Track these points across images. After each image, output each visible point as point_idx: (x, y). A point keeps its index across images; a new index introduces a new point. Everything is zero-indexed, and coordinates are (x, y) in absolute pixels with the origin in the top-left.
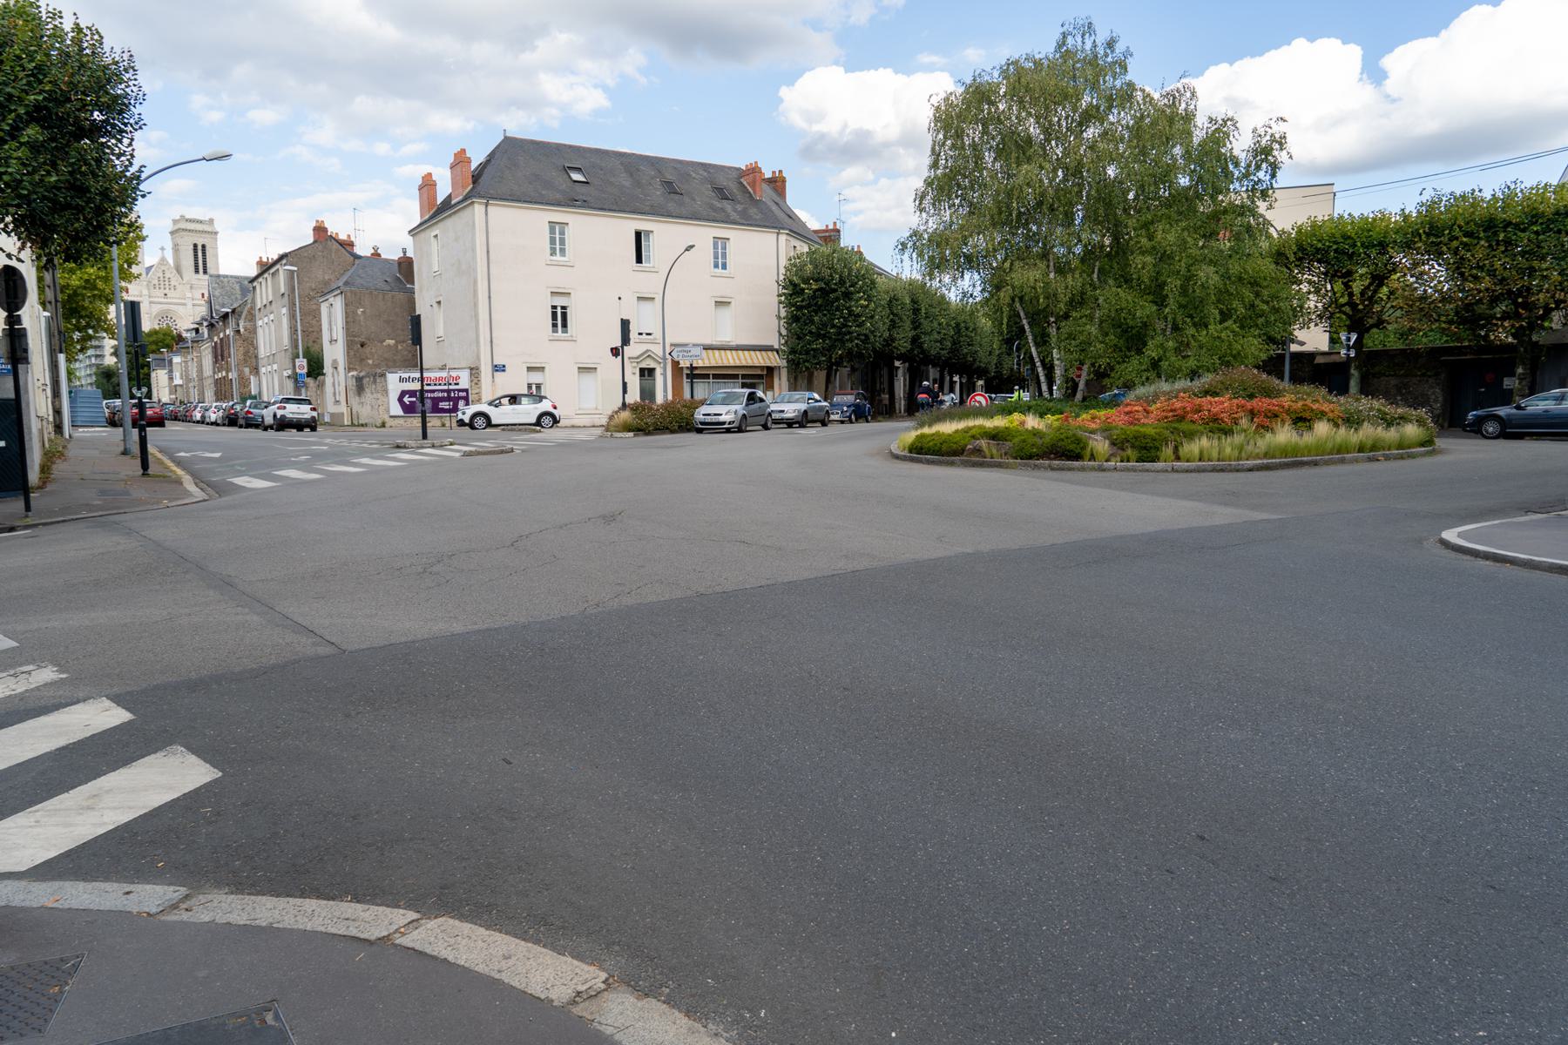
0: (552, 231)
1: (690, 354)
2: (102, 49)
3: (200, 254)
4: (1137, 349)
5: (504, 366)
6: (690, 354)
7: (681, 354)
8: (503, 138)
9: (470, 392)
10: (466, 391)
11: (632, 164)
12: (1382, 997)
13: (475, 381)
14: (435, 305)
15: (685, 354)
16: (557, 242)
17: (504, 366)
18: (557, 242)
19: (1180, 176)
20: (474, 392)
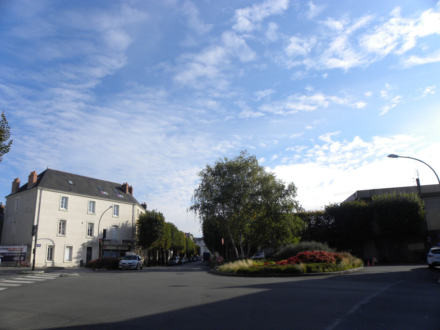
0: (63, 199)
1: (117, 242)
2: (325, 207)
3: (336, 195)
4: (270, 227)
5: (40, 245)
6: (117, 242)
7: (114, 242)
8: (46, 169)
9: (26, 254)
10: (25, 253)
11: (76, 178)
12: (260, 188)
13: (29, 250)
14: (13, 223)
15: (116, 242)
16: (65, 203)
17: (40, 245)
18: (65, 203)
19: (145, 222)
20: (28, 254)
